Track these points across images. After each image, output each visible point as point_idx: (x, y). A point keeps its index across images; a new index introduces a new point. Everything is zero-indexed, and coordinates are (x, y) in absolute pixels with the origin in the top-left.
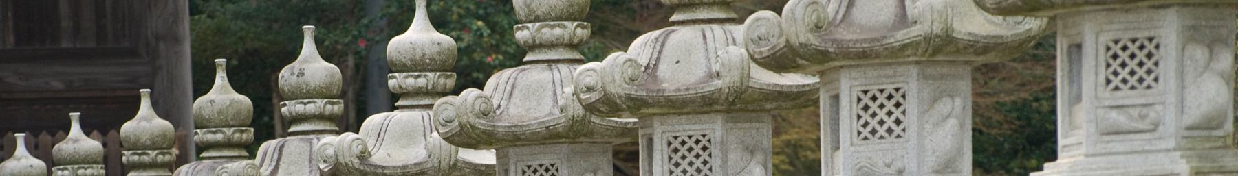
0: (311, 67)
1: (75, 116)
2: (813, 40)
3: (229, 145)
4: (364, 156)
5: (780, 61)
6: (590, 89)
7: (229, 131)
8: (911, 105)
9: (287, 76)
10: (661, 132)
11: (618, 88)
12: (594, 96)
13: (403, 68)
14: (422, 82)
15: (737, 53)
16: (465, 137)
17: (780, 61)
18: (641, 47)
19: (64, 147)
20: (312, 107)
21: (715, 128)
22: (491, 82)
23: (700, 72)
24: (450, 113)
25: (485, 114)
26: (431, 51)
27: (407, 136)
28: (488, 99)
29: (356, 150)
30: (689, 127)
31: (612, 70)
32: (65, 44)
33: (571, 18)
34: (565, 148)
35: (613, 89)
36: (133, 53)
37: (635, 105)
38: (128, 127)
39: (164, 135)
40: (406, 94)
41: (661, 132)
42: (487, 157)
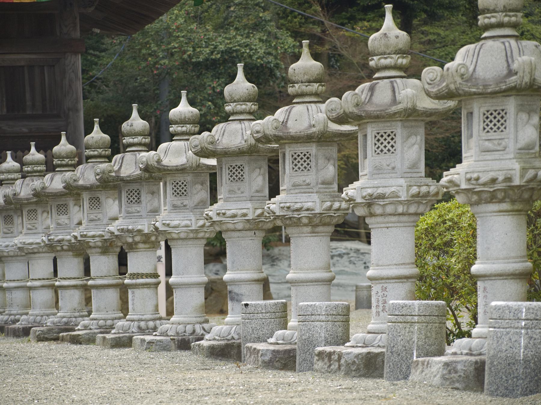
0: (136, 122)
1: (33, 144)
2: (355, 110)
4: (159, 161)
6: (258, 132)
8: (246, 169)
9: (125, 126)
10: (289, 151)
11: (270, 132)
12: (259, 135)
13: (176, 123)
14: (184, 129)
15: (322, 116)
16: (203, 153)
18: (280, 114)
19: (28, 158)
20: (136, 140)
21: (313, 149)
23: (306, 124)
24: (196, 142)
25: (212, 143)
26: (188, 115)
27: (178, 153)
28: (213, 136)
29: (156, 158)
30: (301, 149)
32: (28, 112)
33: (249, 101)
34: (247, 158)
35: (268, 132)
37: (278, 139)
38: (56, 149)
39: (72, 152)
41: (289, 151)
42: (213, 162)
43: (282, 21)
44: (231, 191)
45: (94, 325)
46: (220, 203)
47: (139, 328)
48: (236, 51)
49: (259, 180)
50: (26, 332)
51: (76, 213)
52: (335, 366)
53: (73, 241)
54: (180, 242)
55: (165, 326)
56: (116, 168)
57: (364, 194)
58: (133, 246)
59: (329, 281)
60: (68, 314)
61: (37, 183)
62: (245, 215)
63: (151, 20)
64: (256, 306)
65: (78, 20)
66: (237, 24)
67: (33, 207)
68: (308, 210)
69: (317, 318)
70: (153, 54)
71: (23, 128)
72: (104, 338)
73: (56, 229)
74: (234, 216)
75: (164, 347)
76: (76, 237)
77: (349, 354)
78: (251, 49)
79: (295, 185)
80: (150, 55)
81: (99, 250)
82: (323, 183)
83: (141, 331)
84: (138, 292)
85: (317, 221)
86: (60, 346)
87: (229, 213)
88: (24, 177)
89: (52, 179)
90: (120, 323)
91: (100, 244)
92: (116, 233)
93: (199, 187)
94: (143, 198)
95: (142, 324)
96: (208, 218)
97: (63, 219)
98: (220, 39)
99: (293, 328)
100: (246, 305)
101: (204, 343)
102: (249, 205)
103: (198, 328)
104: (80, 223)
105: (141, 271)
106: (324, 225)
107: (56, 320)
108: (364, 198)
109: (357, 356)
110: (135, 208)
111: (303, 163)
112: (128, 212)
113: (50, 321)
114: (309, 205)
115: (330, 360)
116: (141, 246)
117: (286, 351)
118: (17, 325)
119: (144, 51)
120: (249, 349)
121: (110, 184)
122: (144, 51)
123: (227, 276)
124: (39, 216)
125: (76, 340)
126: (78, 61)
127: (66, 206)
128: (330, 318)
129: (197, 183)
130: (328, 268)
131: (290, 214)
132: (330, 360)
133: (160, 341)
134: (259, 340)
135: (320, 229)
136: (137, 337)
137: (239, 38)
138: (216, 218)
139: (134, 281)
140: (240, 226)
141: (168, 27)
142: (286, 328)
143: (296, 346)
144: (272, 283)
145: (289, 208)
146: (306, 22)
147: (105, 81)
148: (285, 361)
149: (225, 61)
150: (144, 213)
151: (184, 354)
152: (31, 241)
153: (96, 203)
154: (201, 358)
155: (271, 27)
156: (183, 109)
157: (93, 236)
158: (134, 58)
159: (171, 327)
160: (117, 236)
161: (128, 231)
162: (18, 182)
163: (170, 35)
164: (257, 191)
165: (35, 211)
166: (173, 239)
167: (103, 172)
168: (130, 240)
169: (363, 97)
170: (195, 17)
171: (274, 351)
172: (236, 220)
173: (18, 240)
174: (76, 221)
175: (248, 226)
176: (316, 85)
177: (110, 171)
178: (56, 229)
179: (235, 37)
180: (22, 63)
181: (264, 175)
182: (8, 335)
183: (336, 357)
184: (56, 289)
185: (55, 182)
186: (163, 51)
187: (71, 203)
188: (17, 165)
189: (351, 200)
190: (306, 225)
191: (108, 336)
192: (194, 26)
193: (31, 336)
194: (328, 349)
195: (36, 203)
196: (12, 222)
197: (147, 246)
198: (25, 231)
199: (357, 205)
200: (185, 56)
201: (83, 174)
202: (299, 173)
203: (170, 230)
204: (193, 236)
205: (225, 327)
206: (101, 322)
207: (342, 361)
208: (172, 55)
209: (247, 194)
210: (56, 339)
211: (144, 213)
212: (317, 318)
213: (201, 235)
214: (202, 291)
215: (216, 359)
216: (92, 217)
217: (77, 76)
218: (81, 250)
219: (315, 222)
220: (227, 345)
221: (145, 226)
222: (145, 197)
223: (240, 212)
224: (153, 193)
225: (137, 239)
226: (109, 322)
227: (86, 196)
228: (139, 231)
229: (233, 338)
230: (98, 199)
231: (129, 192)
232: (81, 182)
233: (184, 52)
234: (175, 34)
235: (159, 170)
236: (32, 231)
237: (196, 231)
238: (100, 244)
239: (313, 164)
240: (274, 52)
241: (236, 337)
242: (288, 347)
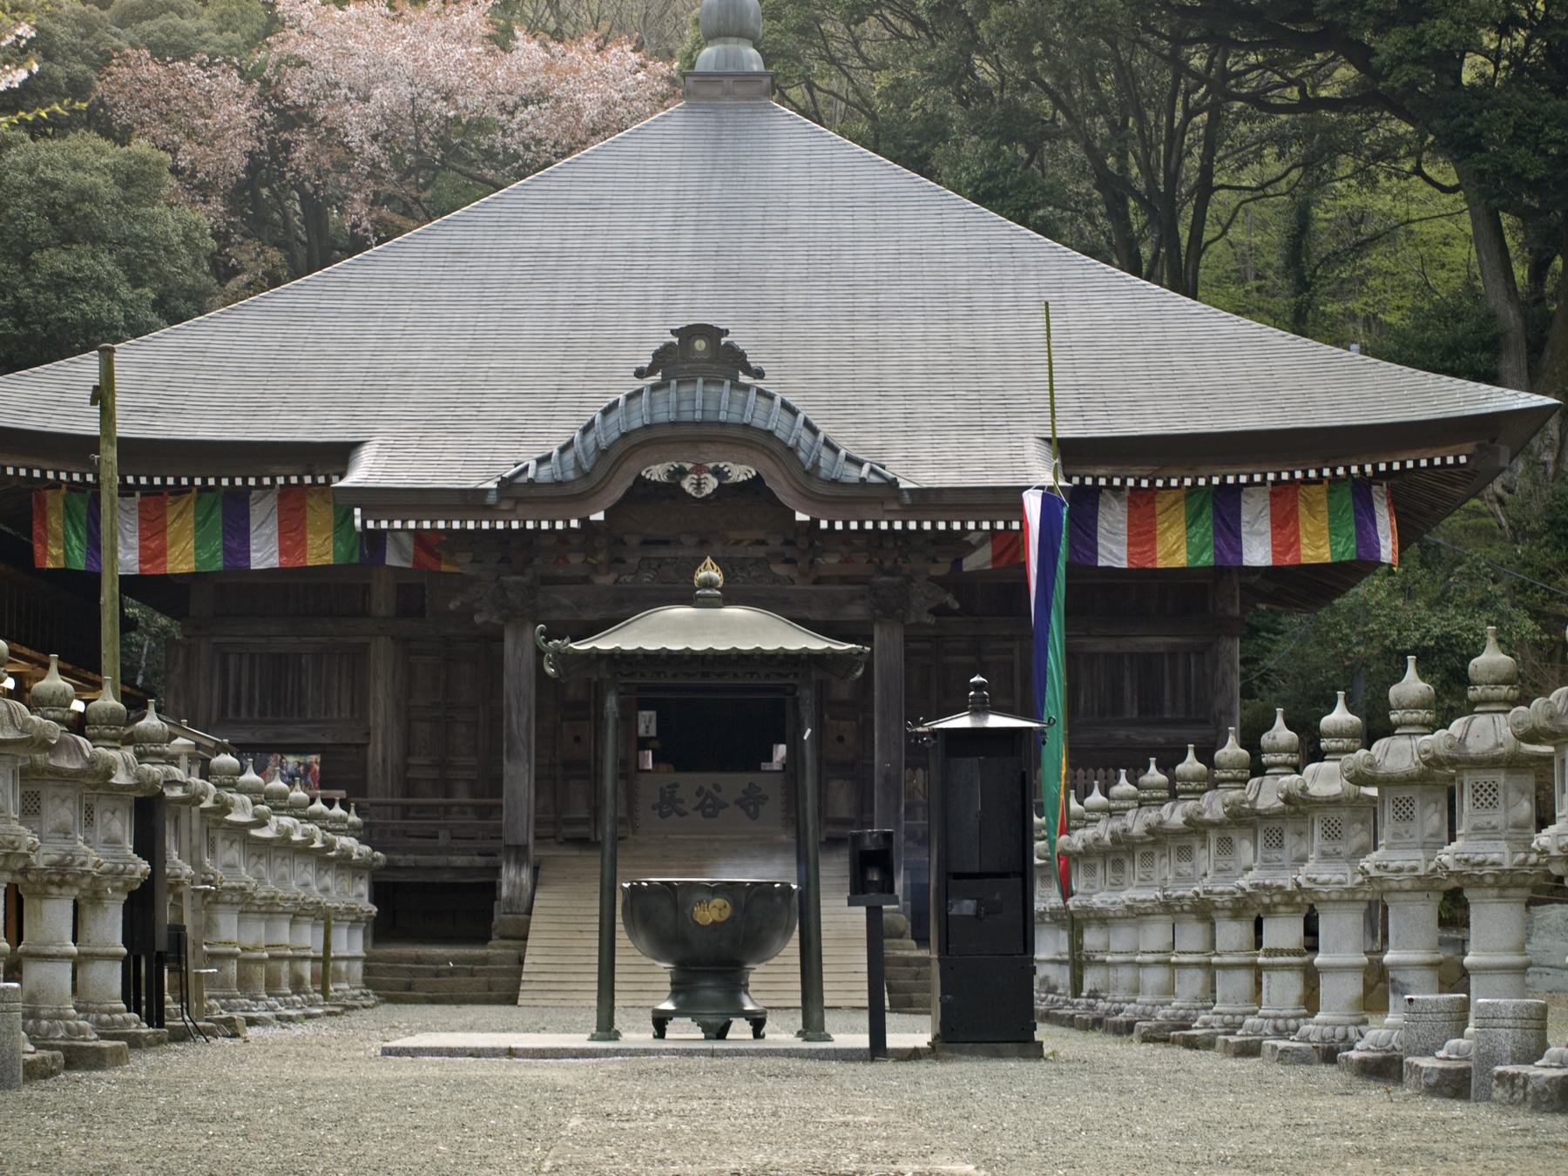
0: (1281, 733)
1: (1153, 760)
2: (1548, 725)
3: (1235, 780)
4: (1304, 789)
5: (1532, 736)
6: (1426, 752)
7: (1285, 756)
8: (1417, 803)
9: (1266, 739)
10: (1468, 780)
11: (1442, 751)
12: (1427, 756)
13: (1329, 736)
14: (1340, 744)
15: (1507, 732)
16: (1358, 779)
17: (1532, 736)
18: (1457, 726)
19: (1145, 779)
20: (1280, 758)
21: (1500, 778)
22: (1375, 745)
23: (1491, 742)
24: (1350, 764)
25: (1370, 766)
26: (1346, 726)
27: (1330, 778)
28: (1372, 757)
29: (1300, 785)
30: (1486, 777)
31: (1437, 740)
32: (1167, 716)
33: (1423, 708)
34: (1418, 788)
35: (1438, 752)
36: (1205, 722)
37: (1453, 762)
38: (1180, 768)
39: (1200, 773)
40: (1224, 781)
41: (1468, 780)
42: (1373, 791)
43: (1519, 597)
44: (1396, 835)
45: (1216, 1021)
46: (1381, 850)
47: (1275, 1028)
48: (1456, 636)
49: (1434, 819)
50: (1128, 1028)
51: (1205, 858)
52: (1519, 1096)
53: (1239, 895)
54: (1331, 905)
55: (1306, 1028)
56: (1251, 797)
57: (1562, 843)
58: (1270, 910)
59: (1522, 969)
60: (1186, 1005)
61: (1151, 816)
62: (1414, 869)
63: (1341, 592)
64: (1423, 1002)
65: (1238, 593)
66: (1458, 600)
67: (1148, 849)
68: (1493, 864)
69: (1501, 1022)
70: (1345, 639)
71: (1159, 736)
72: (1226, 1041)
73: (1176, 880)
74: (1399, 870)
75: (1301, 1058)
76: (1197, 894)
77: (1538, 1077)
78: (1476, 635)
79: (1476, 829)
80: (1341, 640)
81: (1228, 913)
82: (1515, 826)
83: (1279, 1033)
84: (1275, 976)
85: (1505, 880)
86: (1167, 1050)
87: (1392, 865)
88: (1140, 806)
89: (1173, 810)
90: (1249, 1021)
91: (1229, 904)
92: (1249, 890)
93: (1358, 826)
94: (1286, 841)
95: (1280, 1023)
96: (1364, 872)
97: (1185, 867)
98: (1434, 620)
99: (1470, 1038)
100: (1411, 1000)
101: (1354, 1055)
102: (1420, 855)
103: (1352, 1030)
104: (1206, 874)
105: (1281, 945)
106: (1517, 886)
107: (1169, 1012)
108: (1561, 849)
109: (1550, 1080)
110: (1275, 854)
111: (1487, 797)
112: (1265, 861)
113: (1161, 1014)
114: (1495, 857)
115: (1513, 1085)
116: (1282, 909)
117: (1459, 1070)
118: (1120, 1018)
119: (1332, 635)
120: (1410, 1065)
121: (1243, 819)
122: (1332, 635)
123: (1389, 957)
124: (1157, 862)
125: (1191, 1043)
126: (1234, 649)
127: (1189, 848)
128: (1519, 1023)
129: (1356, 821)
130: (1521, 949)
131: (1468, 869)
132: (1513, 1085)
133: (1298, 1049)
134: (1428, 1052)
135: (1511, 892)
136: (1268, 1042)
137: (1460, 618)
138: (1374, 873)
139: (1270, 960)
140: (1407, 885)
141: (1365, 603)
142: (1461, 1036)
143: (1471, 1064)
144: (1048, 1017)
145: (1467, 860)
146: (1551, 599)
147: (1281, 673)
148: (1455, 1085)
149: (1441, 650)
150: (1287, 863)
151: (1325, 1069)
152: (1143, 897)
153: (1226, 845)
154: (1345, 1076)
155: (1504, 605)
156: (1340, 716)
157: (1222, 893)
158: (1320, 643)
159: (1315, 1028)
160: (1249, 894)
161: (1265, 887)
162: (1130, 813)
163: (1368, 612)
164: (1432, 835)
165: (1151, 854)
166: (1321, 901)
167: (1233, 803)
168: (1266, 900)
169: (1559, 707)
170: (1403, 589)
171: (1442, 1070)
172: (1402, 876)
173: (1127, 895)
174: (1202, 871)
175: (1418, 885)
176: (1505, 688)
177: (1243, 802)
178: (1176, 880)
179: (1454, 617)
180: (1162, 649)
181: (1441, 812)
182: (1106, 1031)
183: (1519, 1082)
184: (1209, 968)
185: (1174, 815)
186: (1358, 634)
187: (1197, 845)
188: (1132, 788)
189: (1543, 851)
190: (1491, 886)
191: (1232, 1039)
192: (1400, 602)
193: (1135, 1034)
194: (1511, 1069)
195: (1154, 843)
196: (1122, 870)
197: (1290, 909)
198: (1136, 882)
199: (1552, 859)
200: (1387, 642)
201: (1210, 804)
202: (1482, 811)
203: (1317, 888)
204: (1347, 897)
205: (1384, 1032)
206: (1228, 1018)
207: (1529, 1088)
208: (1371, 639)
209: (1417, 839)
210: (1166, 1040)
211: (1287, 863)
212: (1501, 1022)
213: (1360, 896)
214: (1360, 977)
215: (1369, 1078)
216: (1220, 865)
217: (1233, 668)
218: (1204, 910)
219: (1503, 882)
220: (1385, 1059)
221: (1286, 880)
222: (1289, 840)
223: (1407, 865)
224: (1300, 834)
225: (1277, 899)
226: (1238, 1019)
227: (1213, 836)
228: (1280, 888)
229: (1394, 1048)
230: (1229, 840)
231: (1268, 832)
232: (1207, 816)
233: (1386, 637)
234: (1375, 612)
235: (1304, 801)
236: (1145, 882)
237: (1352, 891)
238: (1229, 904)
239: (1501, 799)
240: (1507, 639)
241: (1398, 1046)
242: (1463, 1065)
